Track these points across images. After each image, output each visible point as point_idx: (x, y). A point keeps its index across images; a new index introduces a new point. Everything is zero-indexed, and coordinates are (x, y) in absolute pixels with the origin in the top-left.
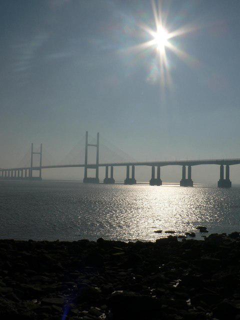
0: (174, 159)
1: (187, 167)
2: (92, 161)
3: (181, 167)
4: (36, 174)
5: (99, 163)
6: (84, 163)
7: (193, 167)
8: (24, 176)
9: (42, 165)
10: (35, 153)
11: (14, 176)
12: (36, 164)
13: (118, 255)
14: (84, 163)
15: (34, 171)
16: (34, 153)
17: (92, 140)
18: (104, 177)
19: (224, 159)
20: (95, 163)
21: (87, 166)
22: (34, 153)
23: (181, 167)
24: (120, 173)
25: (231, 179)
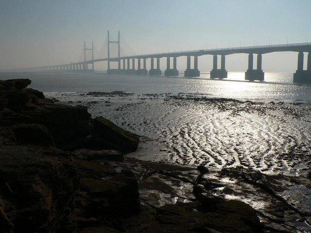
0: (283, 42)
1: (255, 56)
2: (114, 55)
3: (246, 56)
4: (90, 66)
5: (120, 56)
6: (106, 56)
7: (228, 57)
8: (136, 68)
9: (94, 59)
10: (111, 42)
11: (142, 67)
12: (89, 59)
13: (248, 207)
14: (107, 58)
15: (112, 63)
16: (117, 42)
17: (114, 38)
18: (185, 68)
19: (264, 45)
20: (91, 59)
21: (110, 60)
22: (117, 42)
23: (212, 56)
24: (206, 64)
25: (178, 68)
